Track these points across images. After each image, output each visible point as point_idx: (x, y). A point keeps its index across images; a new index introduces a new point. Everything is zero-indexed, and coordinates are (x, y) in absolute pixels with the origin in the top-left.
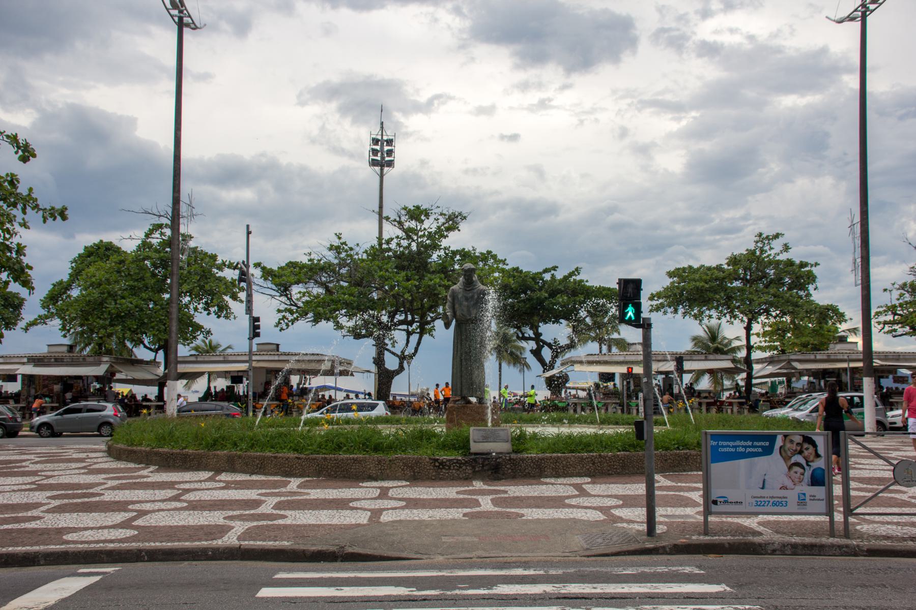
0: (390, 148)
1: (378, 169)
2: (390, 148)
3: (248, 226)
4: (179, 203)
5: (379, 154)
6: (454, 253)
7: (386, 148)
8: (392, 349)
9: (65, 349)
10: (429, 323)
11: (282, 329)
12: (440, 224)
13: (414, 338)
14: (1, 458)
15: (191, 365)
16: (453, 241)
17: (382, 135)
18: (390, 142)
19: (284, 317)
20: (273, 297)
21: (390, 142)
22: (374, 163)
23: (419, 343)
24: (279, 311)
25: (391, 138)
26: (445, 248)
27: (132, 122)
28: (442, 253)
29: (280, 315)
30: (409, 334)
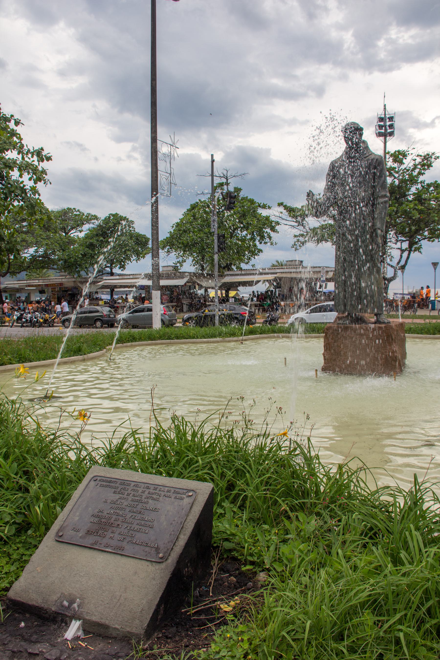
0: (391, 123)
1: (382, 138)
2: (391, 123)
3: (212, 156)
4: (156, 142)
5: (384, 128)
6: (429, 185)
7: (388, 123)
8: (391, 263)
9: (171, 269)
10: (416, 243)
11: (296, 249)
12: (417, 163)
13: (405, 254)
14: (439, 321)
15: (238, 277)
16: (428, 177)
17: (385, 114)
18: (391, 119)
19: (298, 241)
20: (293, 226)
21: (391, 119)
22: (379, 135)
23: (408, 258)
24: (295, 236)
25: (392, 116)
26: (421, 182)
27: (268, 151)
28: (419, 186)
29: (296, 239)
30: (403, 251)
